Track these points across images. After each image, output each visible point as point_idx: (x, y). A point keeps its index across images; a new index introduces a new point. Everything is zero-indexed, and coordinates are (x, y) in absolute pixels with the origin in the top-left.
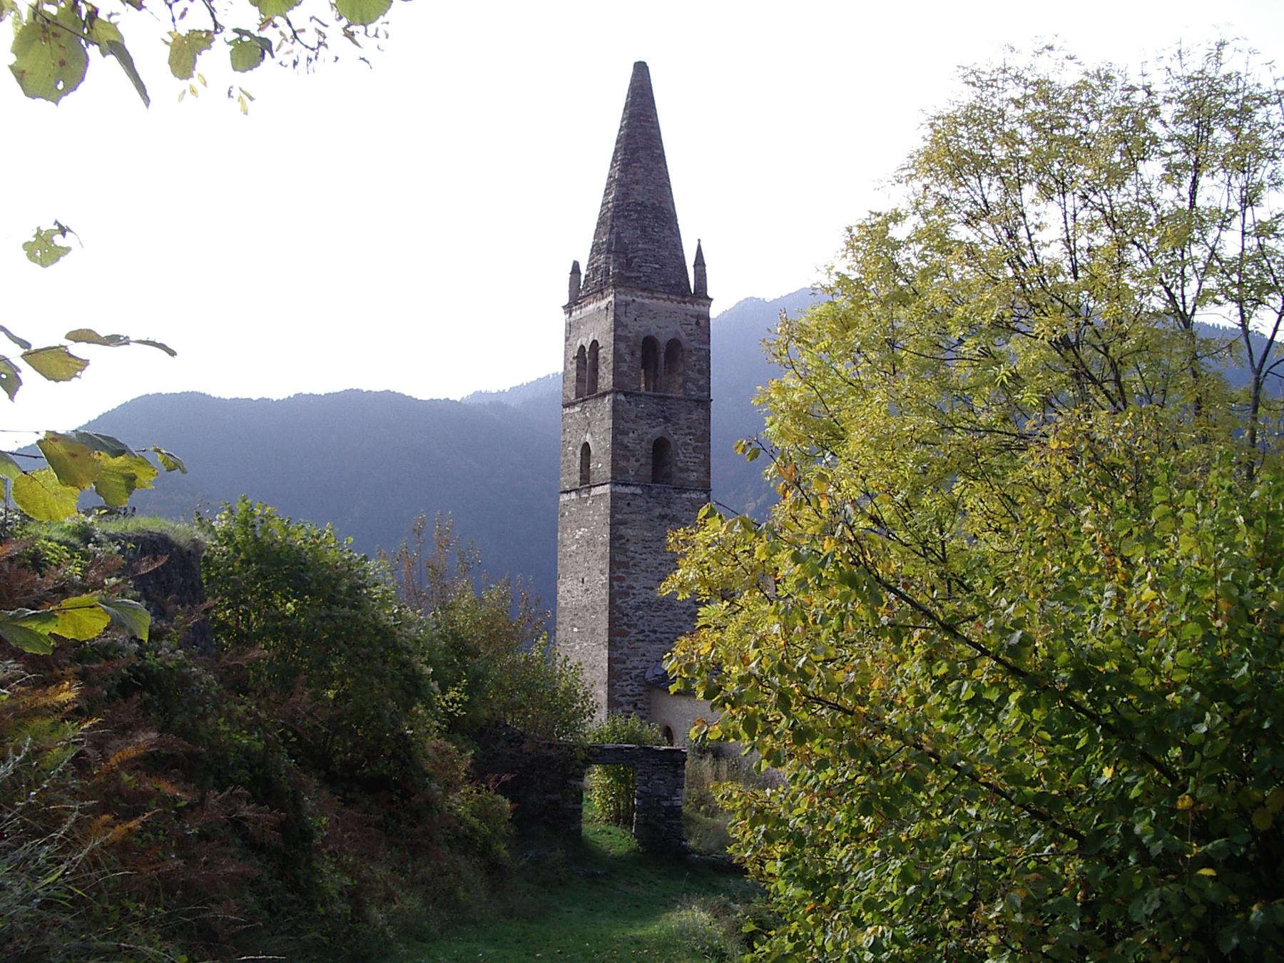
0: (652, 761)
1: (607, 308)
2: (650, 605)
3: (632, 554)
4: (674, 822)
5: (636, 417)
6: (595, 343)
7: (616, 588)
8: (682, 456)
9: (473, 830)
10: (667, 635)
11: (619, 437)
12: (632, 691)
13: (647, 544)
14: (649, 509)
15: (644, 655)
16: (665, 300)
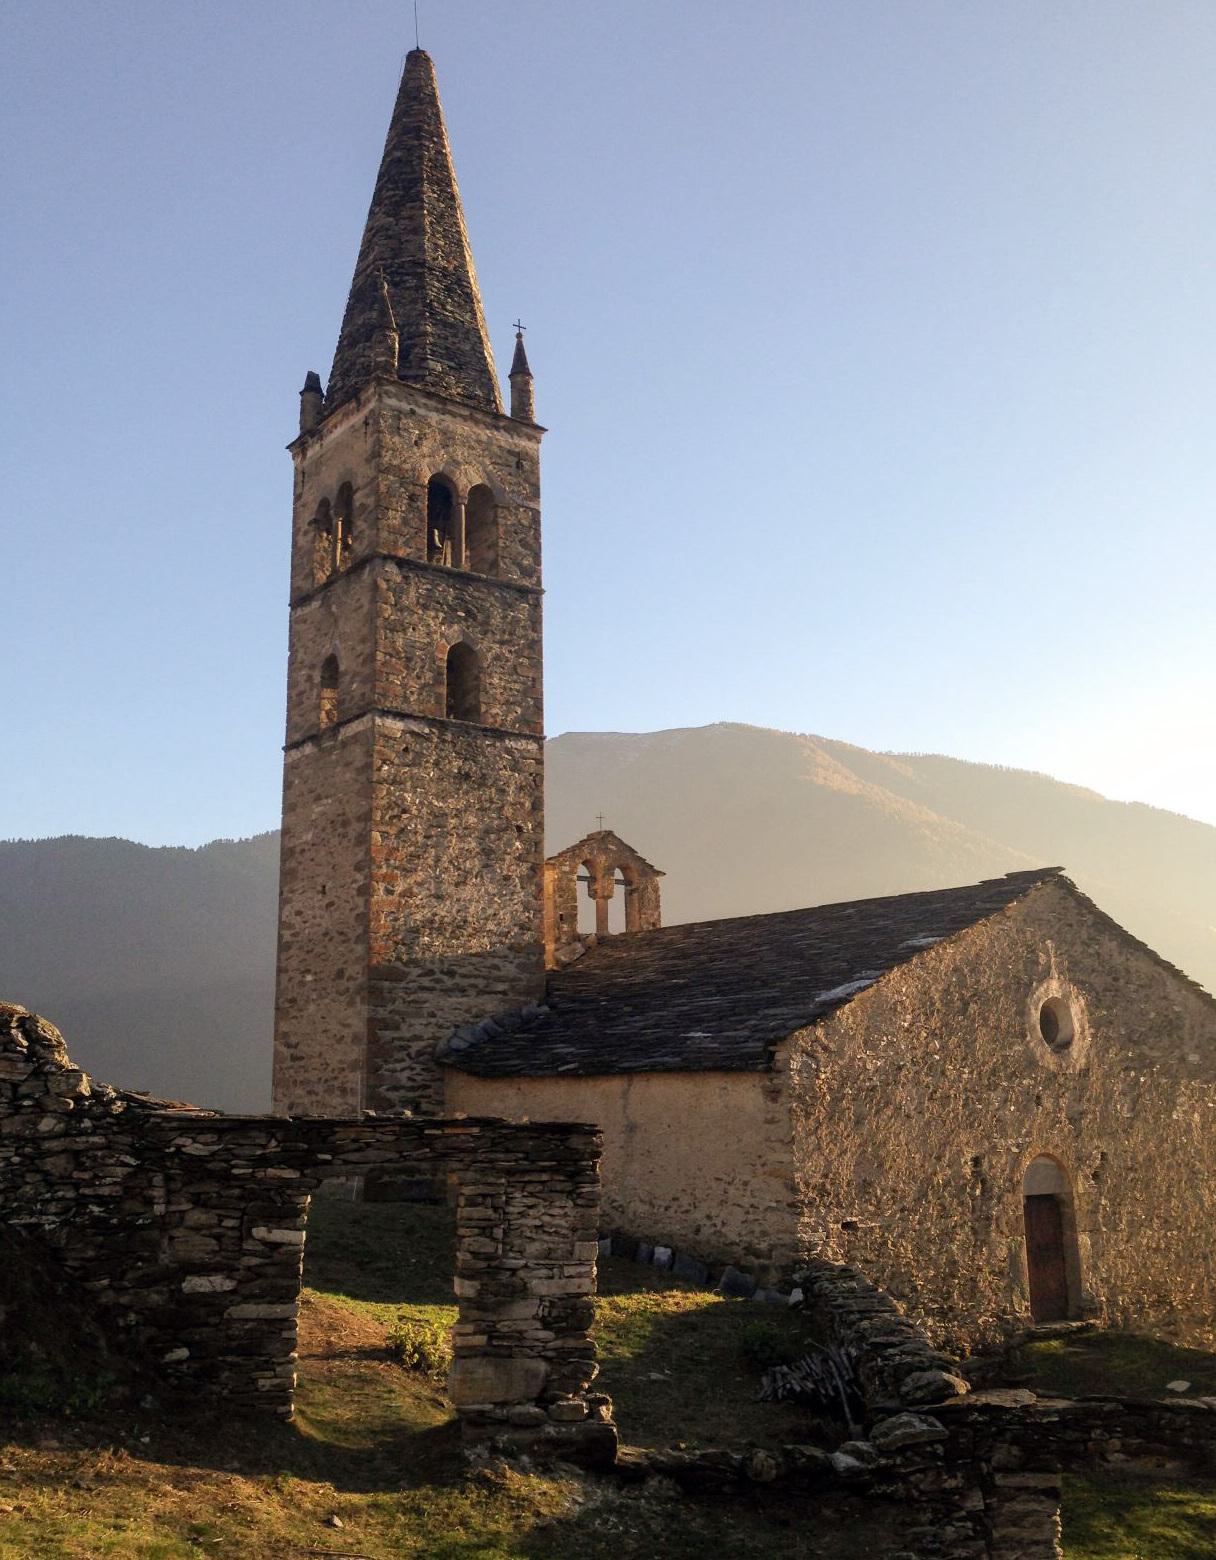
10: (472, 981)
12: (409, 1079)
15: (433, 1015)
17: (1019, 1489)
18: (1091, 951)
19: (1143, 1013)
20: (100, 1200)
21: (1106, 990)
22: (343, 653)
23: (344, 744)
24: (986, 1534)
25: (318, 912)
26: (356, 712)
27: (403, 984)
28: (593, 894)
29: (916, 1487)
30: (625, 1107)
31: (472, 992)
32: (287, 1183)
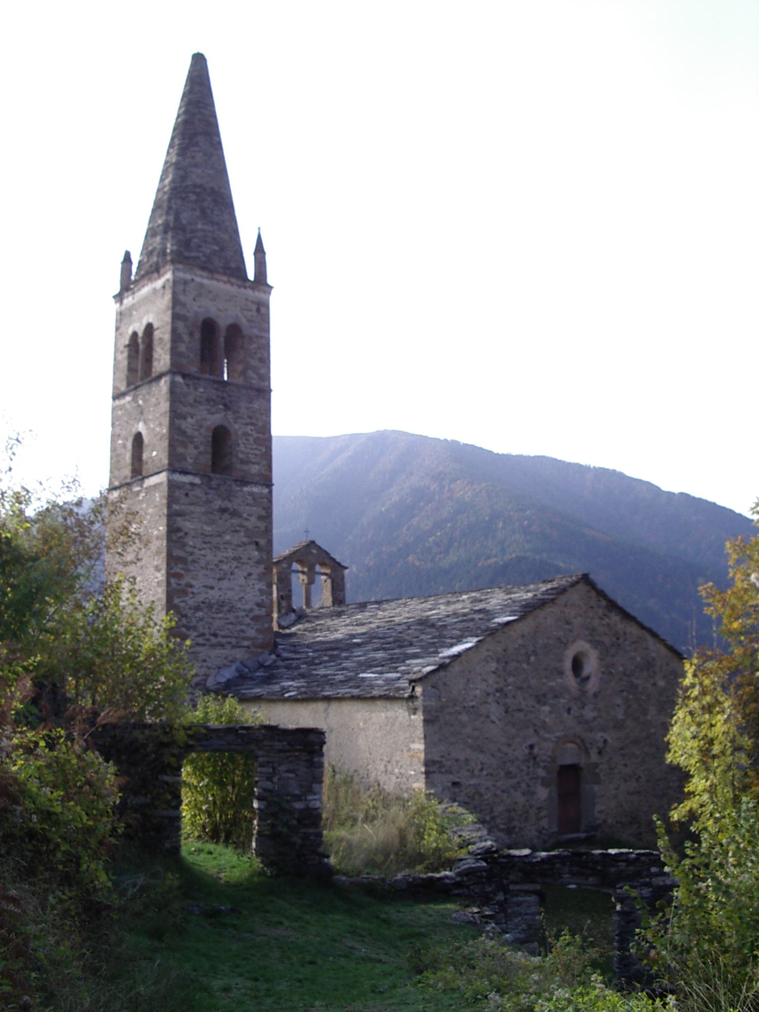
0: (278, 745)
1: (164, 287)
2: (210, 606)
3: (189, 549)
4: (311, 830)
5: (195, 401)
6: (149, 328)
7: (174, 586)
8: (243, 448)
9: (48, 816)
10: (228, 640)
11: (177, 421)
13: (208, 539)
14: (208, 502)
15: (205, 661)
16: (225, 283)
17: (520, 891)
18: (604, 622)
19: (633, 658)
21: (612, 645)
24: (504, 911)
29: (473, 891)
30: (326, 718)
31: (229, 647)
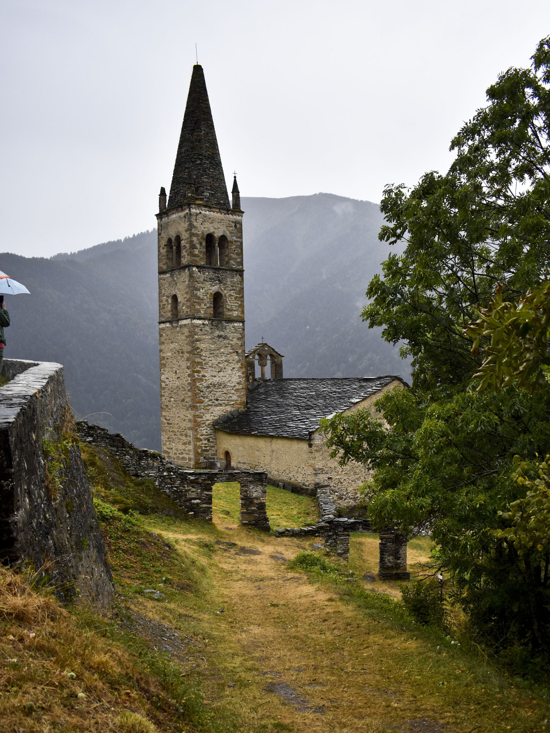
10: (224, 402)
15: (212, 413)
20: (176, 487)
22: (179, 295)
23: (181, 326)
25: (174, 380)
26: (185, 317)
27: (203, 404)
28: (260, 364)
32: (209, 484)
